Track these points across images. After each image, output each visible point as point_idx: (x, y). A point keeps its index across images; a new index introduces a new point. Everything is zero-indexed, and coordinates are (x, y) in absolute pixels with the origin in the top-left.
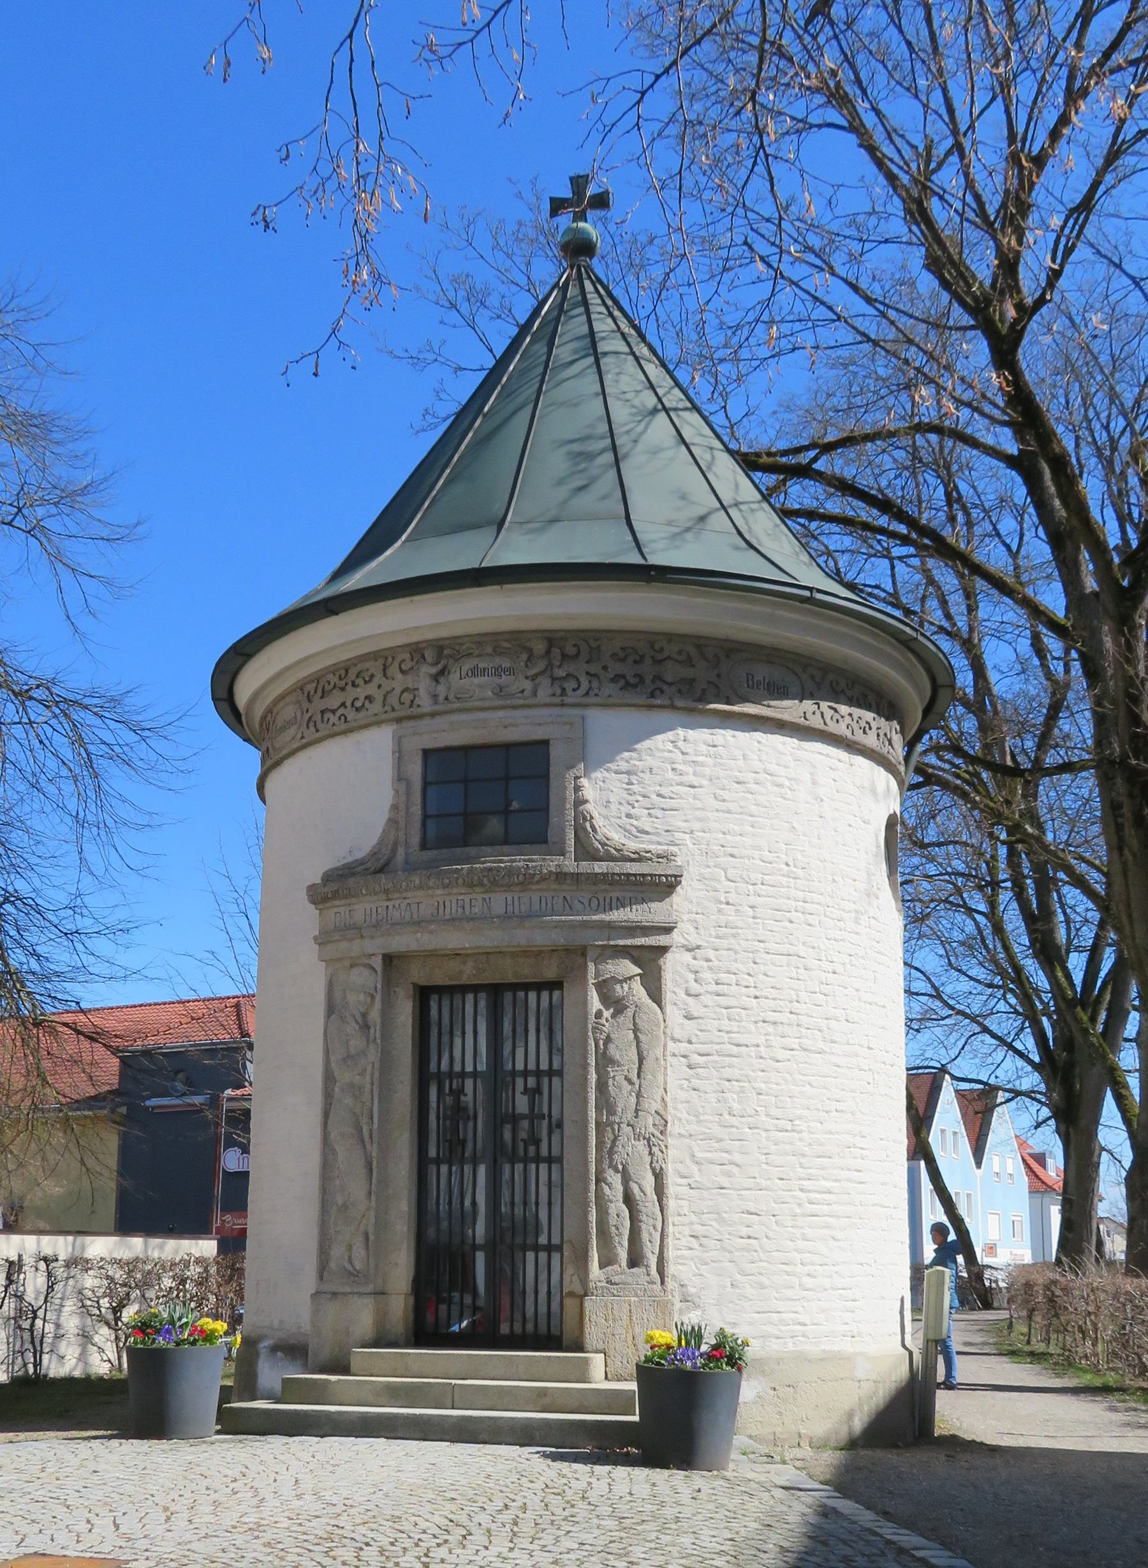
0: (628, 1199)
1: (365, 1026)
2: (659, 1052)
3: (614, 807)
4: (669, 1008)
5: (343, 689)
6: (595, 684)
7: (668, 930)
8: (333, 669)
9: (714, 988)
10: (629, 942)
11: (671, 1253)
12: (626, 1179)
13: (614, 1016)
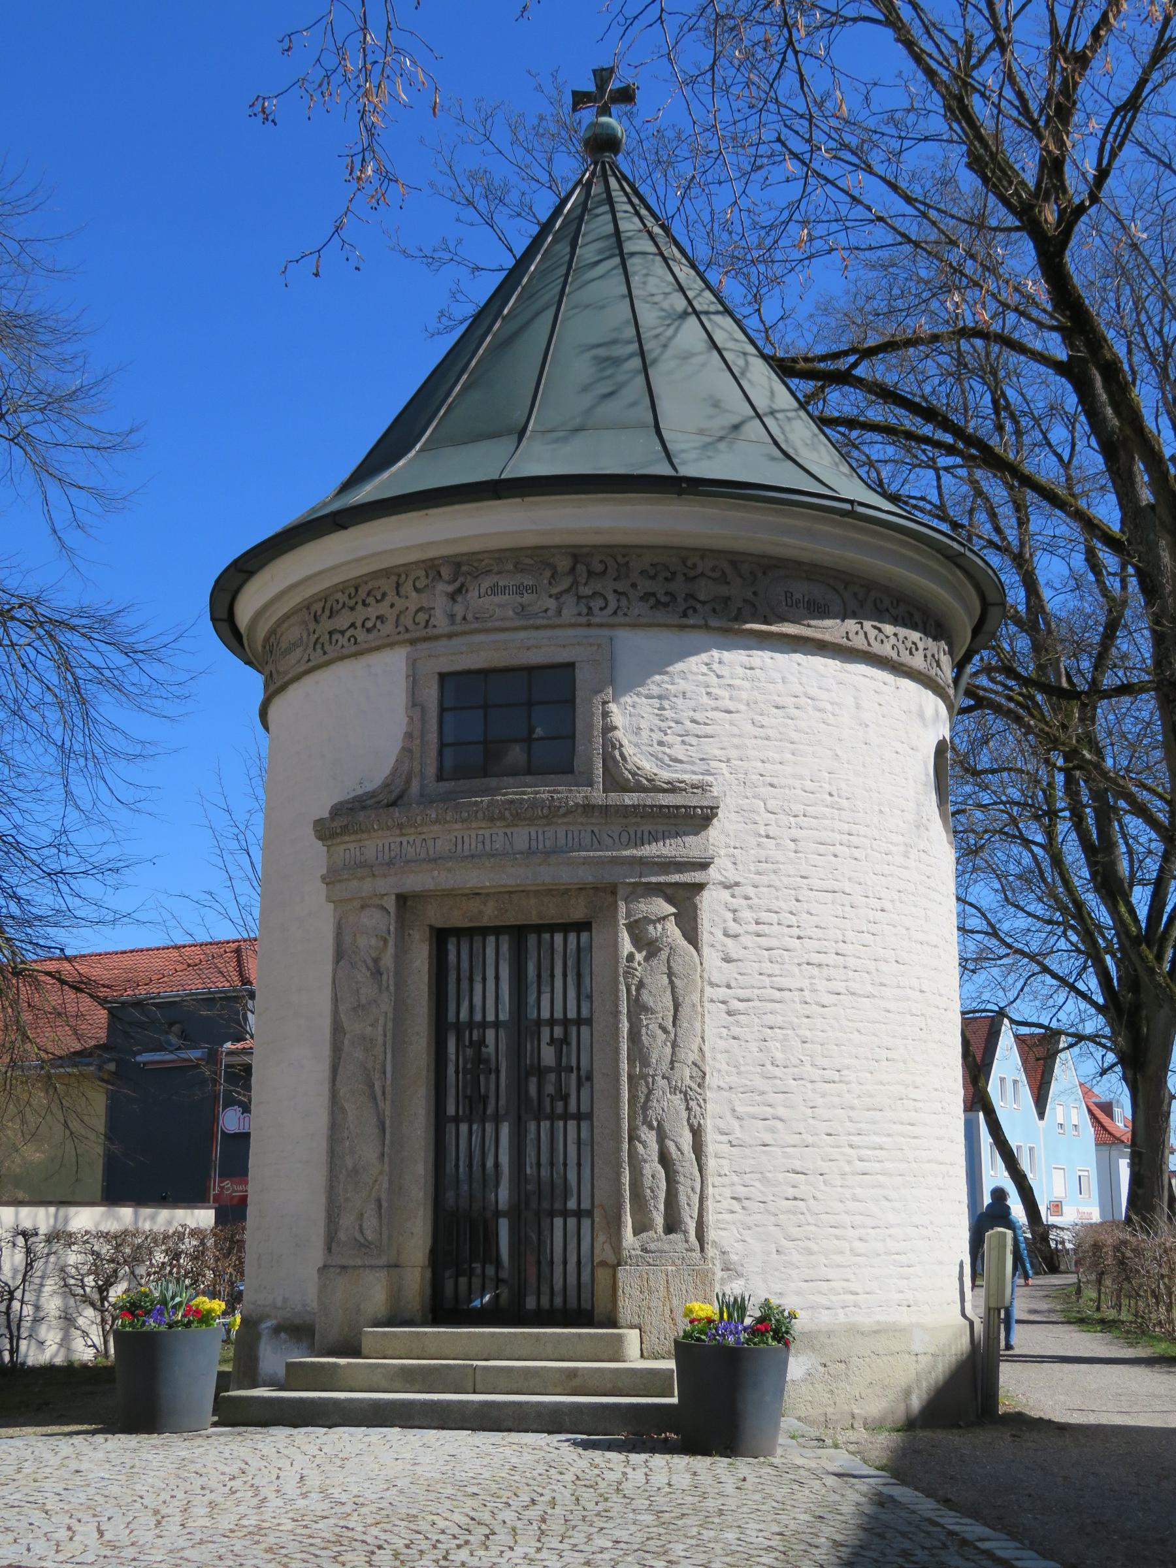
0: (665, 1159)
1: (377, 973)
2: (695, 997)
3: (645, 734)
4: (706, 950)
5: (352, 609)
6: (624, 602)
7: (704, 866)
8: (342, 587)
9: (753, 928)
11: (711, 1218)
12: (662, 1137)
13: (646, 959)
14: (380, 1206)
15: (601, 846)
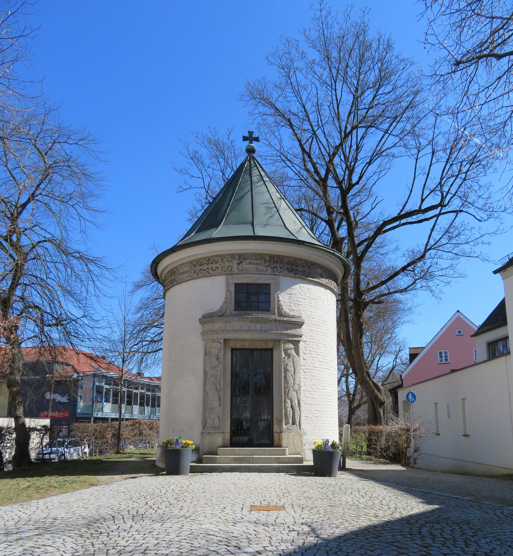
0: (292, 407)
1: (218, 359)
2: (298, 368)
3: (286, 303)
4: (300, 357)
5: (207, 264)
6: (282, 270)
7: (301, 336)
8: (204, 258)
9: (309, 352)
10: (292, 339)
11: (302, 421)
12: (291, 402)
13: (288, 358)
14: (219, 417)
15: (278, 330)
